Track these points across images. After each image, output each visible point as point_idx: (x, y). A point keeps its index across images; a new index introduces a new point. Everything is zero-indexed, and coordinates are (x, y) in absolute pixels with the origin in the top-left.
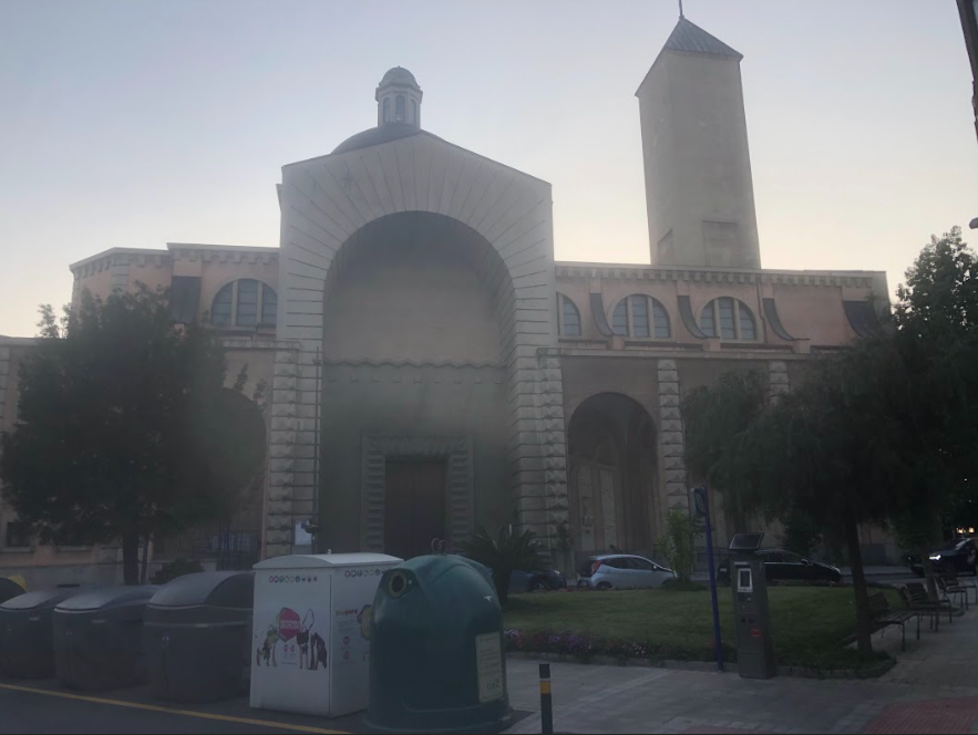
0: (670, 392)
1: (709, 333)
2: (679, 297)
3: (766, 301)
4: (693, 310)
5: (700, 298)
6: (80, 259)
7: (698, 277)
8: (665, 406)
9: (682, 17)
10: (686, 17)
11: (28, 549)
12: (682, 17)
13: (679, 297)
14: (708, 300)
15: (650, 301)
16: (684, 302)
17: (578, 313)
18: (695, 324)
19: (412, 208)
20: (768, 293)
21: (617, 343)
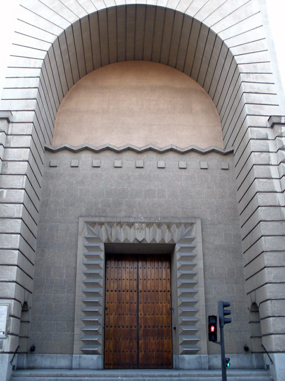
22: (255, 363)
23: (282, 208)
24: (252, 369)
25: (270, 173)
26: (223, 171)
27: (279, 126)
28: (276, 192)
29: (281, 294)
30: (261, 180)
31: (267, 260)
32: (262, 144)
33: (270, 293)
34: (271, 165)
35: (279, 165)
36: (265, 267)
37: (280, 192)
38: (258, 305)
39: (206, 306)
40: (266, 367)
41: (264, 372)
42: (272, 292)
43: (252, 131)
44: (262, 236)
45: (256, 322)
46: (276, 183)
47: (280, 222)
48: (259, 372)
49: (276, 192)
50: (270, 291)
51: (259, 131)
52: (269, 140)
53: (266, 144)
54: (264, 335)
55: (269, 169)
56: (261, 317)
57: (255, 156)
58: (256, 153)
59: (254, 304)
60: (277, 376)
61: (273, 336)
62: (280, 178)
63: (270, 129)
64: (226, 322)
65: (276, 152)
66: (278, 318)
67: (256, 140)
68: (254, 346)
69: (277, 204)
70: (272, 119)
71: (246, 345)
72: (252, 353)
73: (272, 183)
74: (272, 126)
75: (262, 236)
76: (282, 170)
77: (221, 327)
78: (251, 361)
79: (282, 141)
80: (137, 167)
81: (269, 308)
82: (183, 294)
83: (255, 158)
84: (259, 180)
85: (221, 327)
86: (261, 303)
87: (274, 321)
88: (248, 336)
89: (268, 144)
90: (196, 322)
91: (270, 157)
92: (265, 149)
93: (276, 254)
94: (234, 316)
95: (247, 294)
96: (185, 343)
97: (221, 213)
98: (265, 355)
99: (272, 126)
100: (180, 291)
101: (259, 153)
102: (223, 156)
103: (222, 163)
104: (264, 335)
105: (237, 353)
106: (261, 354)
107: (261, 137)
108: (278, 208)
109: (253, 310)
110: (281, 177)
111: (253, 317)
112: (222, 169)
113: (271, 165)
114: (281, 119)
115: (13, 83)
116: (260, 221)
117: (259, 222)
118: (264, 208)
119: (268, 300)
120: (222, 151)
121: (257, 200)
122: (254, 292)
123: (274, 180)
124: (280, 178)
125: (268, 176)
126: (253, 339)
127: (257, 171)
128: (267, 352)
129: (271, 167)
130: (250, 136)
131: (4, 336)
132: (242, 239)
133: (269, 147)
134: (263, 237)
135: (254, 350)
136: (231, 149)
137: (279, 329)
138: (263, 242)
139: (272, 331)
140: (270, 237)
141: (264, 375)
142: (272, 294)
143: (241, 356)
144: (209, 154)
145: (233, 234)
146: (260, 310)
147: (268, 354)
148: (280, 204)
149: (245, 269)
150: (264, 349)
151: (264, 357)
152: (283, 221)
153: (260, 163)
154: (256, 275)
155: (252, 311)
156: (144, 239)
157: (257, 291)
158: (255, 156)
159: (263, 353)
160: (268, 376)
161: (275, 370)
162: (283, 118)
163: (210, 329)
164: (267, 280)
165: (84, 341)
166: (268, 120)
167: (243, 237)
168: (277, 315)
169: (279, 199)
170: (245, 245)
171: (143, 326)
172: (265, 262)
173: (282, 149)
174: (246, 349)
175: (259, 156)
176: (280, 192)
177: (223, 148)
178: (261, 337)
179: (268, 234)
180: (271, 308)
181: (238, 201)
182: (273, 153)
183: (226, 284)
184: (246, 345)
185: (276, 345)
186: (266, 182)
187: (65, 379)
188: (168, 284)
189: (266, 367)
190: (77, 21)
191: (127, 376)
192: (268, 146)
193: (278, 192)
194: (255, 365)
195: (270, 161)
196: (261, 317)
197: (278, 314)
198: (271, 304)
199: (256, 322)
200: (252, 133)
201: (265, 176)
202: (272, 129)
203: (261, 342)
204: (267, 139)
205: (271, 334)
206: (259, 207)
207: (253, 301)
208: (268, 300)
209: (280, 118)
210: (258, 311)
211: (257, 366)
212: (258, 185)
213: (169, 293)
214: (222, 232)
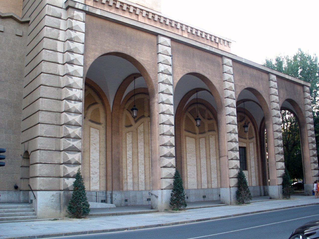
0: (229, 81)
8: (162, 72)
22: (22, 198)
23: (60, 77)
24: (19, 203)
25: (57, 46)
26: (17, 37)
27: (73, 9)
28: (58, 63)
29: (48, 146)
30: (48, 51)
31: (42, 117)
32: (55, 21)
33: (40, 144)
34: (59, 40)
35: (65, 42)
36: (39, 123)
37: (61, 64)
38: (29, 154)
40: (30, 202)
41: (28, 205)
42: (42, 144)
43: (49, 8)
44: (40, 98)
45: (26, 167)
46: (60, 56)
47: (57, 88)
48: (24, 205)
49: (58, 63)
50: (40, 143)
51: (55, 10)
52: (62, 19)
53: (59, 22)
54: (31, 177)
55: (57, 44)
56: (31, 163)
57: (47, 30)
58: (48, 28)
59: (26, 152)
60: (38, 208)
61: (38, 178)
62: (64, 53)
63: (65, 11)
65: (65, 31)
66: (44, 165)
67: (50, 17)
68: (22, 185)
69: (57, 73)
70: (68, 3)
71: (16, 184)
72: (21, 190)
73: (57, 55)
74: (67, 9)
75: (40, 98)
76: (67, 47)
78: (19, 197)
79: (72, 23)
81: (38, 156)
83: (47, 32)
84: (46, 50)
86: (32, 152)
87: (41, 166)
88: (19, 177)
89: (60, 22)
91: (59, 34)
92: (56, 26)
93: (49, 113)
94: (9, 161)
95: (22, 143)
97: (9, 72)
98: (30, 192)
99: (67, 9)
101: (51, 28)
102: (19, 24)
103: (18, 30)
104: (31, 177)
105: (8, 191)
106: (27, 192)
107: (55, 16)
108: (58, 76)
109: (25, 157)
110: (65, 52)
111: (24, 163)
112: (17, 35)
113: (59, 40)
114: (76, 4)
116: (41, 85)
117: (40, 86)
118: (46, 74)
119: (38, 150)
120: (20, 20)
121: (41, 67)
122: (27, 142)
123: (59, 54)
124: (64, 53)
125: (54, 49)
126: (22, 180)
127: (46, 43)
128: (32, 191)
129: (58, 42)
130: (47, 12)
132: (24, 97)
133: (60, 25)
134: (41, 99)
135: (22, 188)
136: (28, 19)
137: (44, 173)
138: (41, 103)
139: (38, 174)
140: (47, 99)
141: (28, 207)
142: (41, 145)
143: (11, 193)
144: (7, 19)
145: (16, 92)
146: (30, 157)
147: (33, 192)
148: (60, 74)
149: (22, 122)
150: (31, 188)
151: (30, 194)
152: (59, 88)
153: (50, 37)
154: (31, 128)
155: (24, 158)
157: (30, 141)
158: (47, 30)
159: (30, 190)
160: (31, 208)
161: (36, 203)
162: (77, 4)
164: (39, 134)
166: (65, 3)
167: (24, 96)
168: (43, 162)
169: (60, 69)
170: (25, 102)
172: (40, 119)
173: (71, 29)
174: (16, 188)
175: (51, 31)
176: (61, 64)
177: (21, 16)
178: (29, 179)
179: (46, 96)
180: (40, 157)
181: (26, 65)
182: (63, 31)
183: (5, 133)
184: (16, 184)
185: (40, 185)
186: (51, 54)
187: (8, 214)
189: (30, 202)
191: (11, 211)
192: (60, 24)
193: (60, 64)
194: (22, 200)
195: (58, 36)
196: (31, 163)
197: (44, 161)
198: (40, 153)
199: (27, 166)
200: (48, 10)
201: (52, 49)
202: (66, 11)
203: (29, 182)
204: (60, 18)
205: (37, 177)
206: (42, 73)
207: (26, 150)
208: (38, 150)
209: (75, 3)
210: (29, 158)
211: (23, 200)
212: (45, 55)
214: (7, 89)
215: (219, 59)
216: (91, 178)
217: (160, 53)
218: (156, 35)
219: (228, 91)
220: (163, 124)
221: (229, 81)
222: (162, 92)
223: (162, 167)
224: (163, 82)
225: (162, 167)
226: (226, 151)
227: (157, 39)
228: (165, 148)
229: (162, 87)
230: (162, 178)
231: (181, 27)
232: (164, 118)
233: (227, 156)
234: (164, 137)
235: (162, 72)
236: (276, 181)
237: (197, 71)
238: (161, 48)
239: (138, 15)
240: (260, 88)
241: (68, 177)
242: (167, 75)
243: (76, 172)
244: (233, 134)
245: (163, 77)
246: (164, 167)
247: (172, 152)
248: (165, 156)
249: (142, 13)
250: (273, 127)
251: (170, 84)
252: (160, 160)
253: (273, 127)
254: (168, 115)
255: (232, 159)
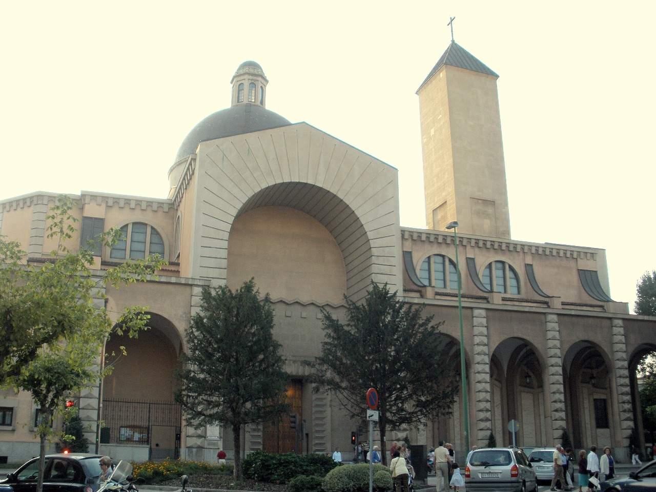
0: (554, 339)
1: (426, 283)
2: (467, 259)
3: (527, 265)
4: (478, 268)
5: (482, 260)
6: (5, 199)
7: (481, 244)
8: (477, 344)
9: (453, 41)
10: (456, 42)
11: (10, 428)
12: (453, 41)
13: (467, 259)
14: (487, 263)
15: (507, 267)
16: (470, 262)
17: (163, 244)
18: (416, 275)
19: (287, 180)
20: (529, 260)
21: (430, 292)
39: (331, 420)
64: (360, 435)
77: (357, 437)
80: (302, 318)
82: (317, 412)
85: (357, 437)
90: (324, 431)
96: (317, 444)
100: (314, 410)
115: (207, 252)
131: (218, 439)
156: (292, 372)
163: (352, 438)
165: (251, 442)
171: (282, 432)
188: (300, 402)
190: (312, 185)
213: (301, 408)
215: (542, 317)
216: (418, 440)
217: (475, 326)
218: (472, 308)
219: (552, 350)
220: (479, 391)
221: (554, 339)
222: (478, 363)
223: (478, 430)
224: (478, 354)
225: (478, 430)
226: (550, 411)
227: (472, 312)
228: (481, 413)
229: (478, 358)
230: (478, 440)
231: (523, 249)
232: (480, 387)
233: (551, 417)
234: (480, 404)
235: (477, 344)
236: (111, 431)
237: (516, 335)
238: (476, 321)
239: (465, 246)
240: (598, 338)
241: (398, 440)
242: (482, 346)
243: (405, 436)
244: (558, 394)
245: (478, 349)
246: (481, 430)
247: (488, 416)
248: (481, 420)
249: (470, 242)
250: (616, 380)
251: (485, 354)
252: (477, 423)
253: (616, 380)
254: (484, 384)
255: (556, 420)
